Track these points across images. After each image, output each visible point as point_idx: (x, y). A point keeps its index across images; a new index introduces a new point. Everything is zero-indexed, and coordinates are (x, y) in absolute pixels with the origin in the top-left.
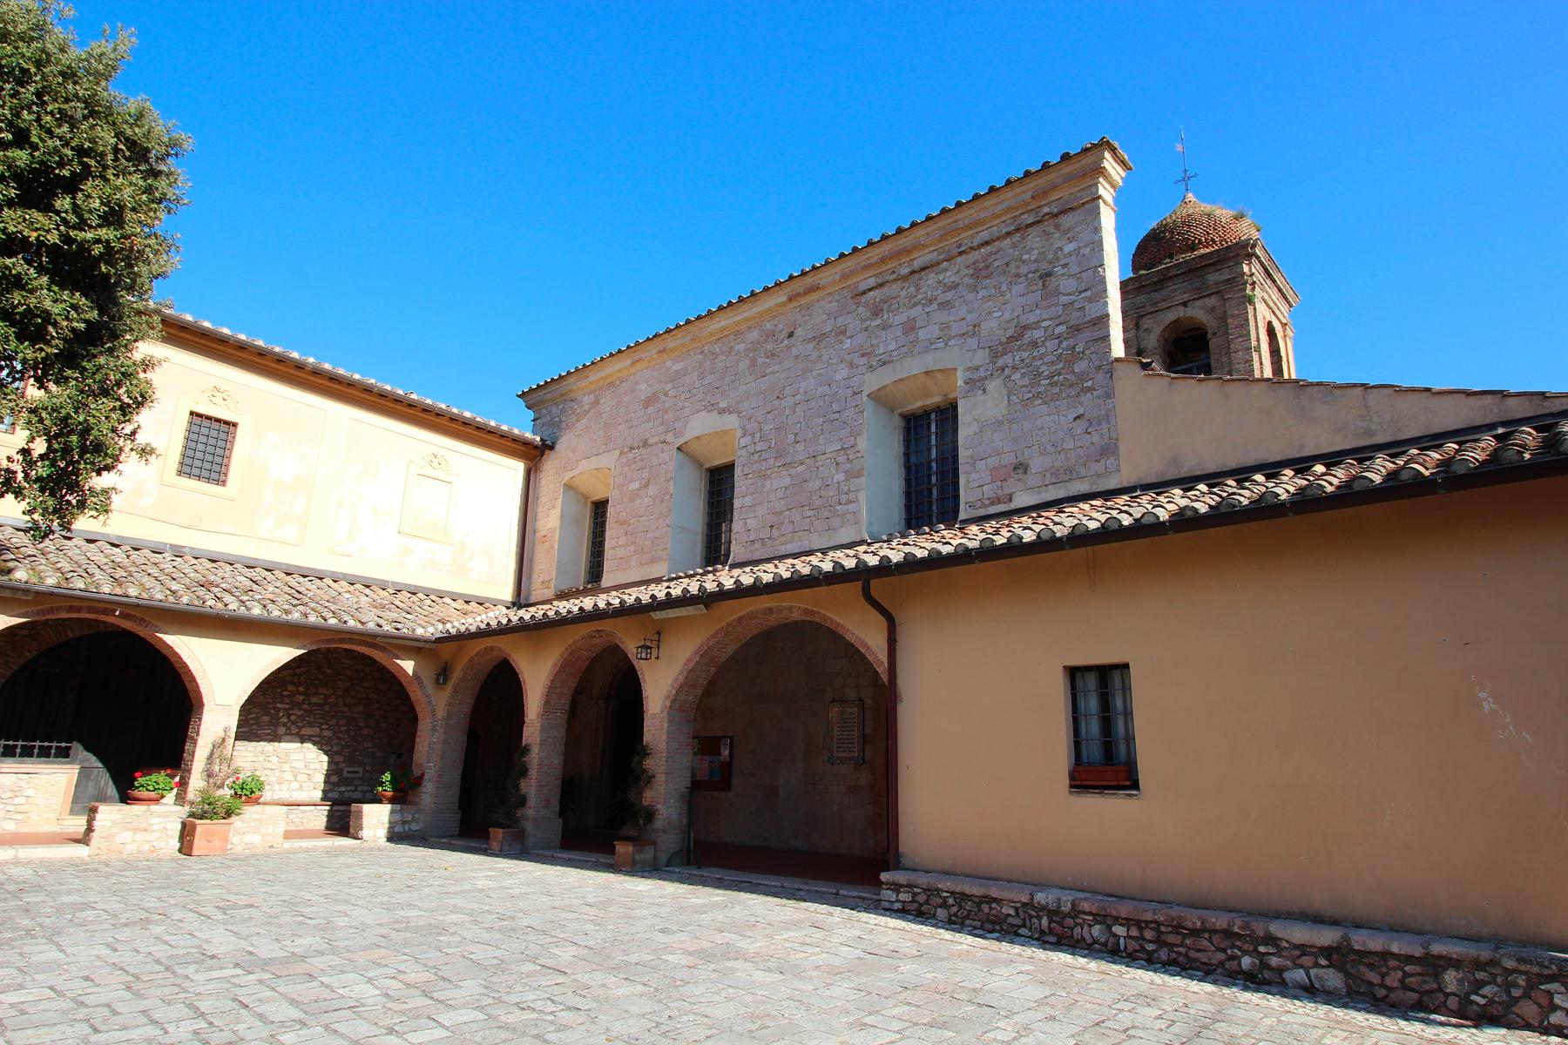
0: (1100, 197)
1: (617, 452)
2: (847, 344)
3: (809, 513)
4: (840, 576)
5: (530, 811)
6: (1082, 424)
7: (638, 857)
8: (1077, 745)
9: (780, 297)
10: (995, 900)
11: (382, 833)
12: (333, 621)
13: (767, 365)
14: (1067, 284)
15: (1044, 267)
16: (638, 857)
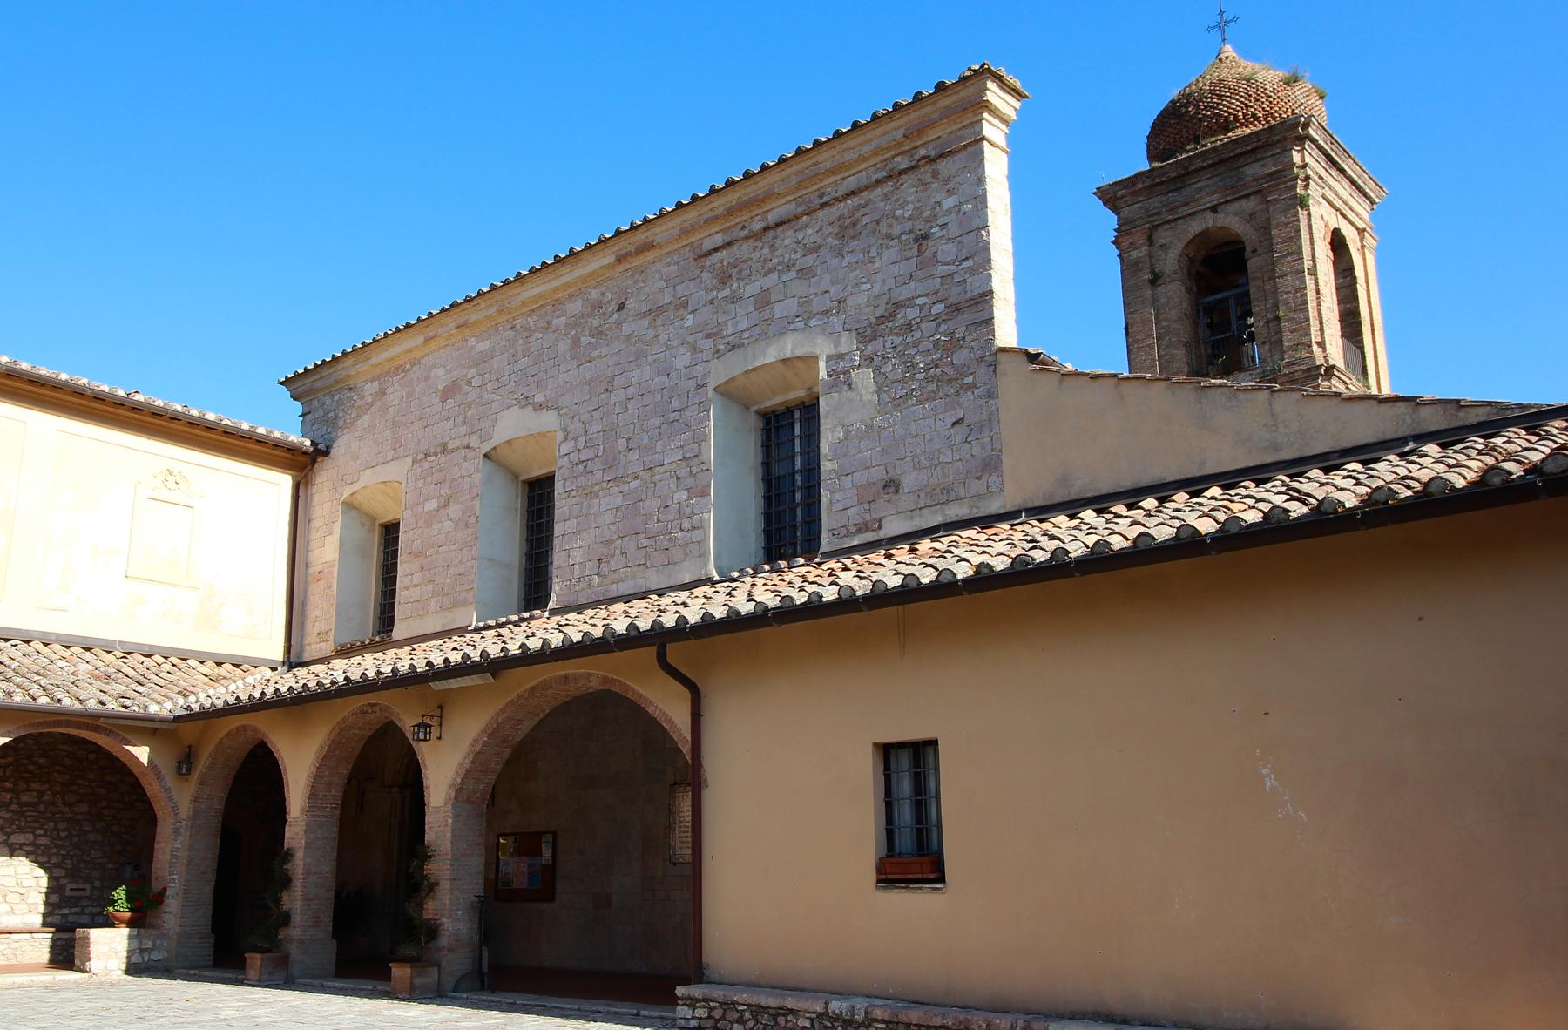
0: (983, 138)
1: (409, 460)
2: (690, 321)
3: (645, 543)
4: (634, 639)
5: (295, 931)
6: (961, 431)
7: (418, 981)
8: (890, 833)
9: (606, 258)
10: (792, 1011)
11: (120, 962)
12: (43, 701)
13: (593, 347)
14: (947, 251)
15: (920, 226)
16: (418, 981)
